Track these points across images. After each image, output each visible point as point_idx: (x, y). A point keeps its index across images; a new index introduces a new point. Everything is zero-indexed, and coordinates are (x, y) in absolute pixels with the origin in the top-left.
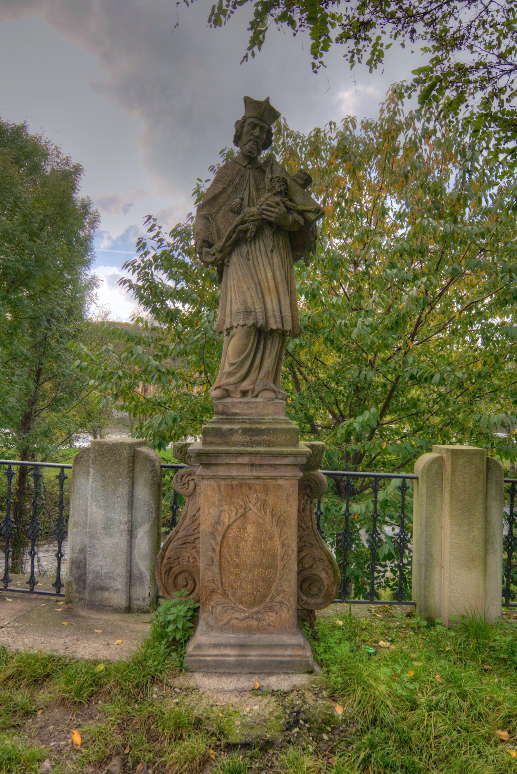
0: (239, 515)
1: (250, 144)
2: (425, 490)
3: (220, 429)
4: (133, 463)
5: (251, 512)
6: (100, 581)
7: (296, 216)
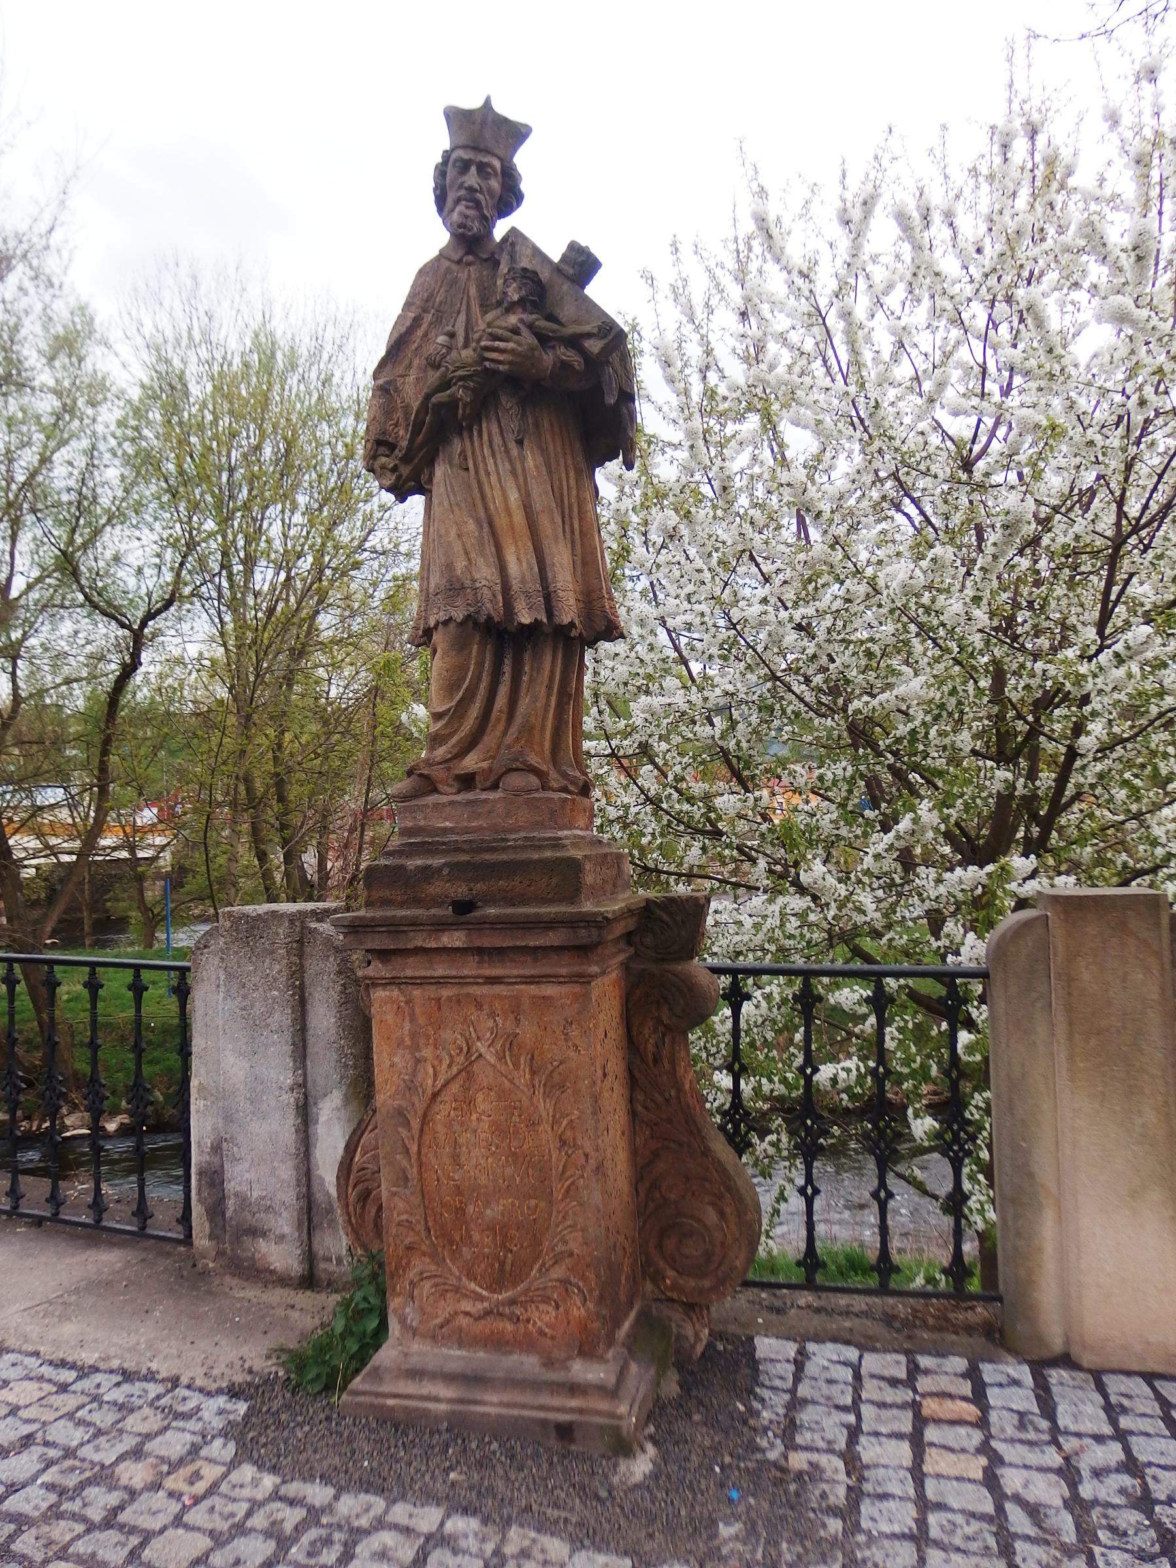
0: (455, 1070)
1: (460, 208)
3: (402, 868)
4: (301, 956)
5: (481, 1062)
6: (249, 1217)
7: (566, 354)
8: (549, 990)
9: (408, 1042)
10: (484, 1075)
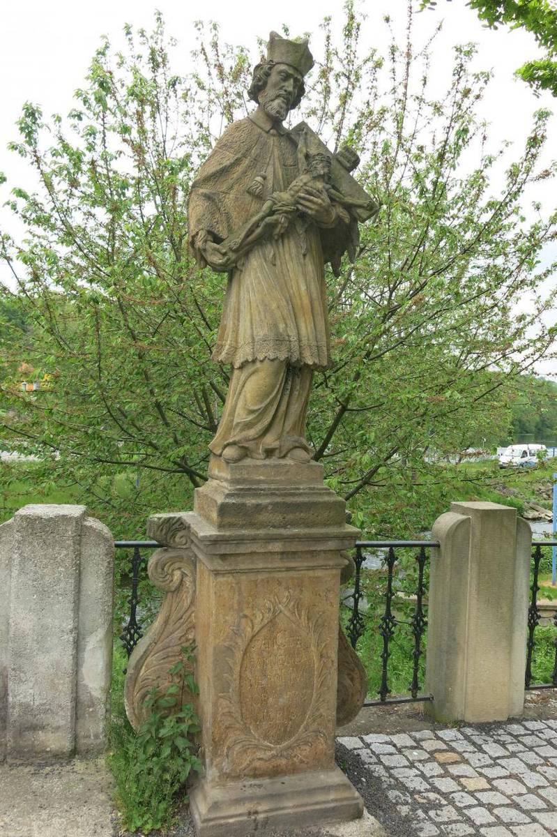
2: (448, 561)
3: (244, 505)
5: (282, 615)
6: (30, 718)
7: (340, 211)
8: (319, 573)
9: (236, 606)
10: (282, 622)
